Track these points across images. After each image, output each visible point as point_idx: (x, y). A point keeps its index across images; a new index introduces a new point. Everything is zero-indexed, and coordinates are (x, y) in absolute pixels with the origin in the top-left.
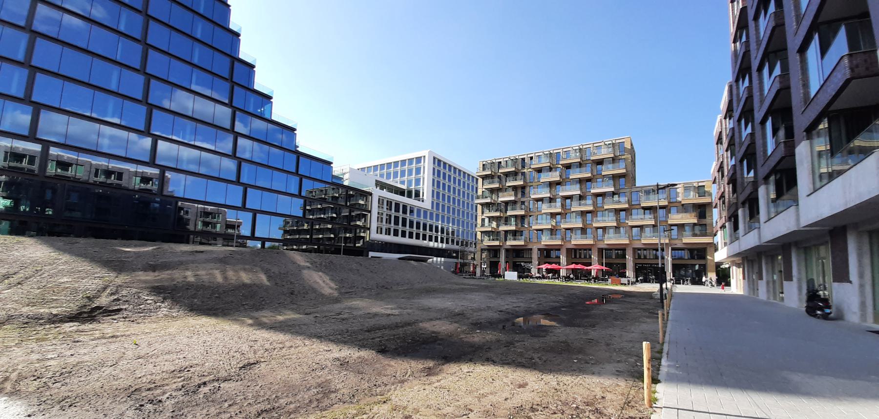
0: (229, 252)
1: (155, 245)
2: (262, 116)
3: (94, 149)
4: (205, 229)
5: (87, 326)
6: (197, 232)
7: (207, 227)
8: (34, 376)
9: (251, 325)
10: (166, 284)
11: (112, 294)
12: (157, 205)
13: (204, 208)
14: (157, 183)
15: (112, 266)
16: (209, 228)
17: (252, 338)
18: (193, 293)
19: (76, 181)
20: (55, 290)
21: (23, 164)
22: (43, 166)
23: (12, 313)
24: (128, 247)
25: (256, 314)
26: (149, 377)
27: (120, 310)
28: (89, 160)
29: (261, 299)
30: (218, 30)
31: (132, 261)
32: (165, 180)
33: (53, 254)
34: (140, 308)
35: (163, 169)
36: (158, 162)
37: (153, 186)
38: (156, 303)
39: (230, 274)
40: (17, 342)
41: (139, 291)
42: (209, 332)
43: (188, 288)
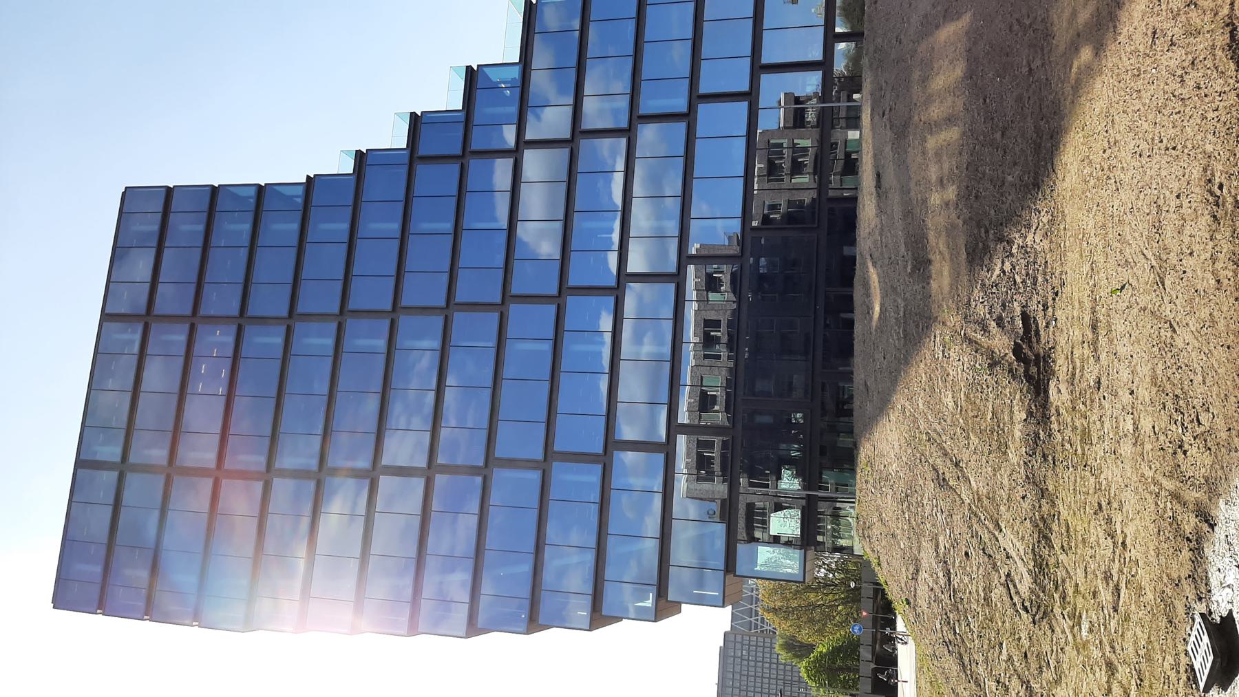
0: (877, 117)
1: (864, 264)
2: (519, 84)
3: (667, 367)
4: (810, 169)
5: (1061, 366)
6: (820, 184)
7: (806, 165)
8: (1175, 453)
9: (1099, 49)
10: (961, 241)
11: (985, 329)
12: (763, 261)
13: (759, 176)
14: (715, 266)
15: (917, 333)
16: (808, 160)
17: (1141, 42)
18: (988, 185)
19: (731, 385)
20: (971, 414)
21: (714, 455)
22: (716, 430)
23: (1020, 478)
24: (869, 308)
25: (1062, 38)
26: (1219, 265)
27: (1025, 317)
28: (689, 369)
29: (1016, 27)
30: (369, 193)
31: (905, 299)
32: (705, 252)
33: (892, 417)
34: (1024, 282)
35: (684, 258)
36: (672, 268)
37: (725, 274)
38: (1011, 255)
39: (936, 111)
40: (1088, 474)
41: (979, 286)
42: (1106, 145)
43: (976, 197)
